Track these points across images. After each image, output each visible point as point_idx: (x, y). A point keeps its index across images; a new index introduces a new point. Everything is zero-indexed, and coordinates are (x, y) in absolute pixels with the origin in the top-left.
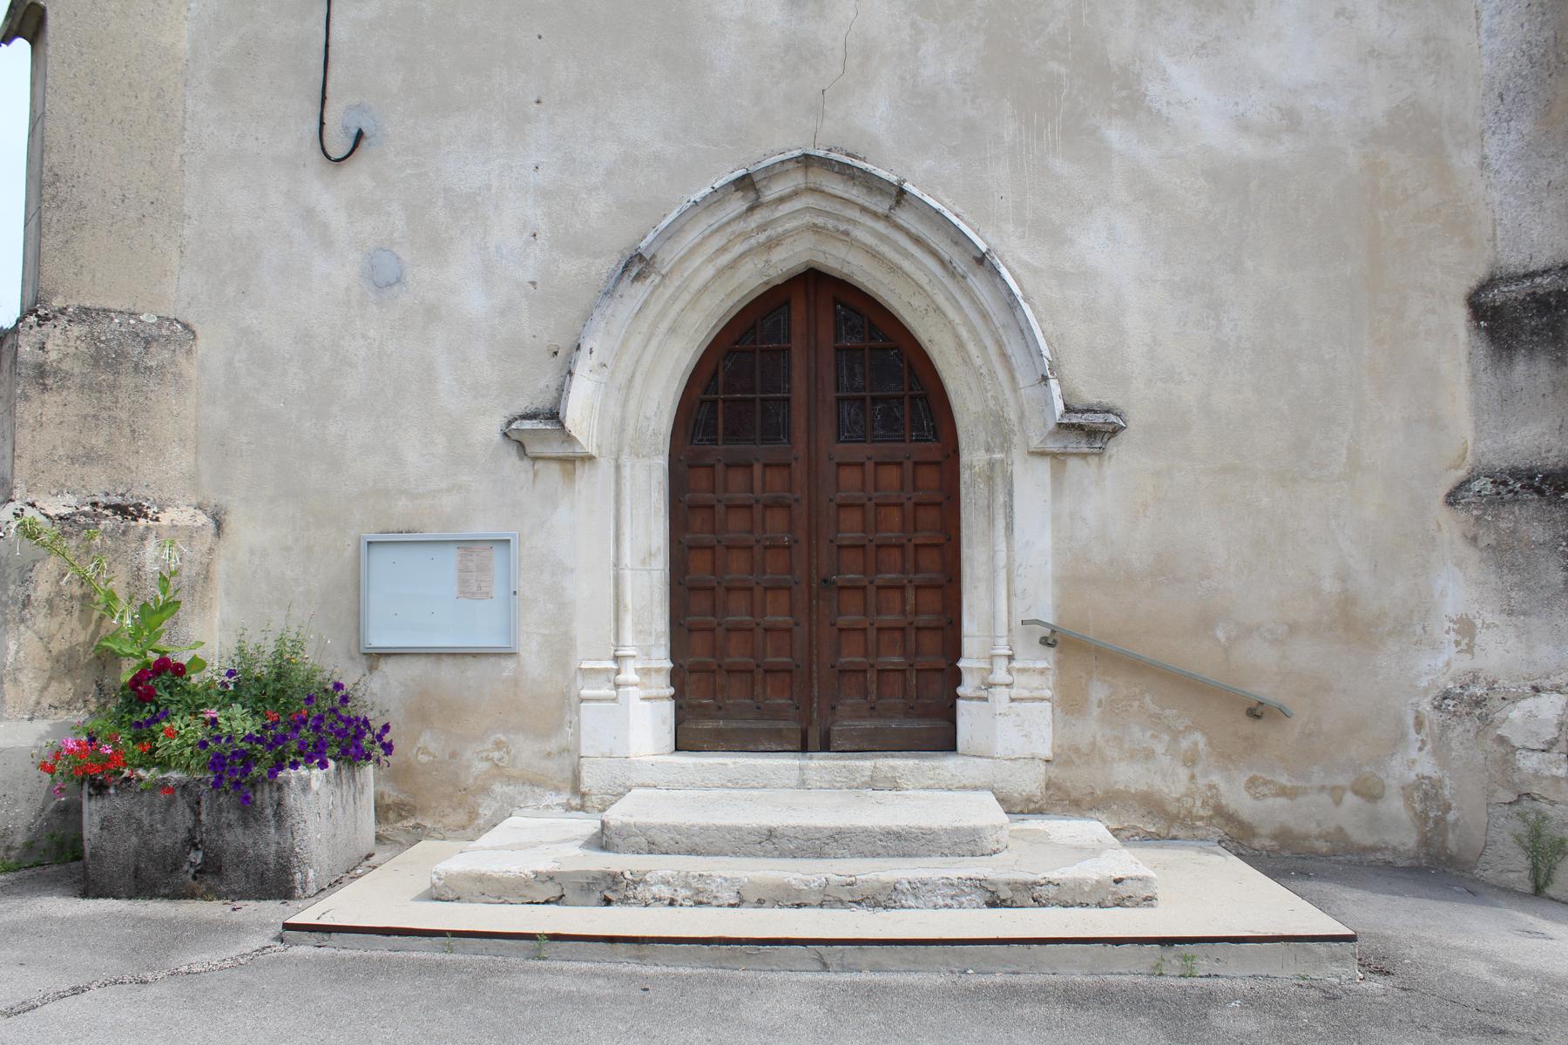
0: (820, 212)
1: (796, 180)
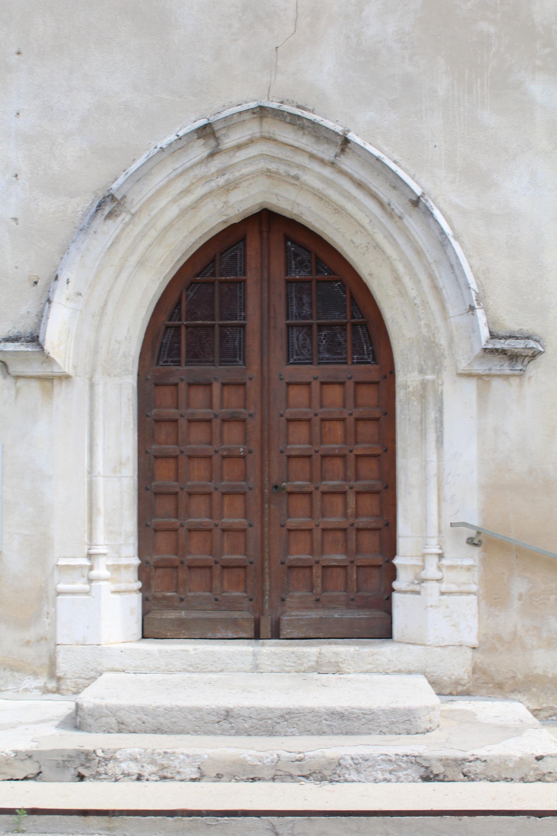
0: (273, 158)
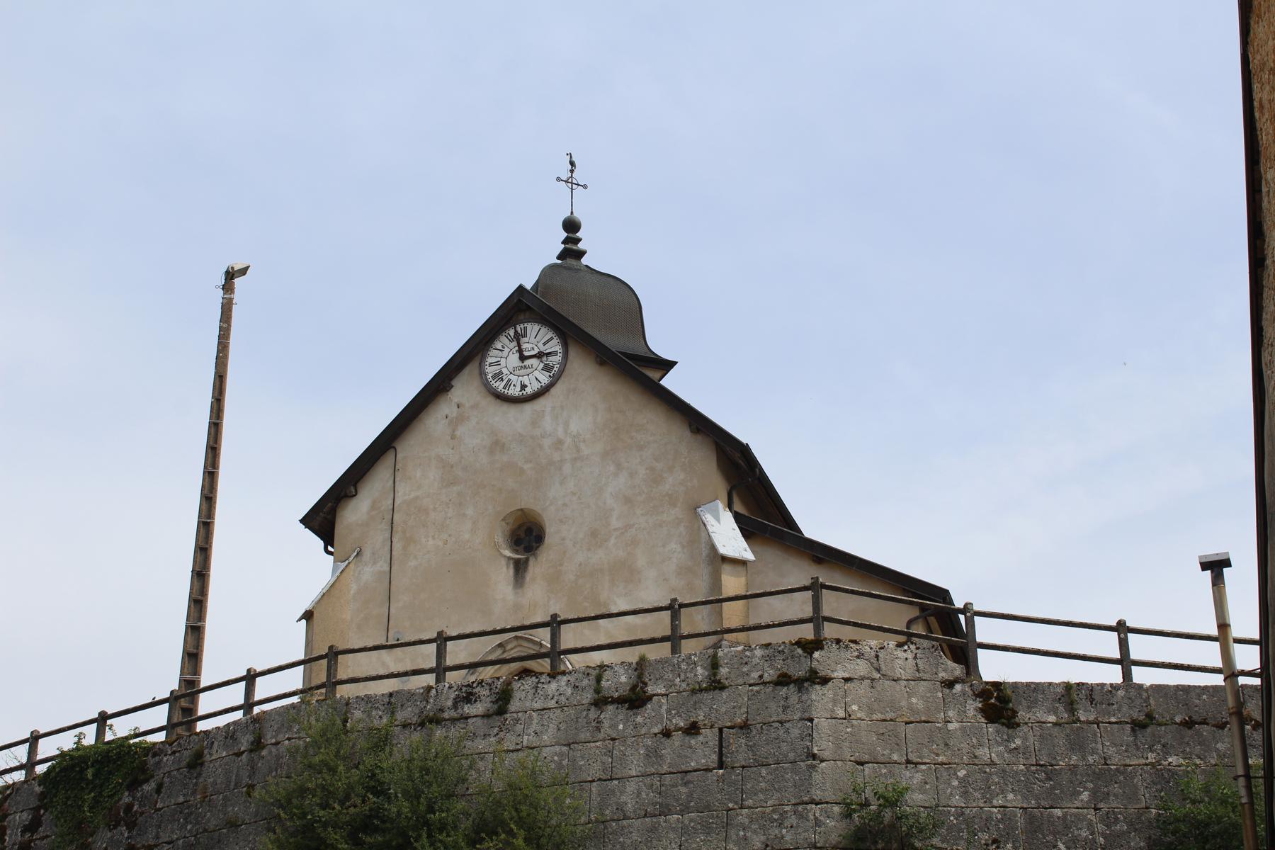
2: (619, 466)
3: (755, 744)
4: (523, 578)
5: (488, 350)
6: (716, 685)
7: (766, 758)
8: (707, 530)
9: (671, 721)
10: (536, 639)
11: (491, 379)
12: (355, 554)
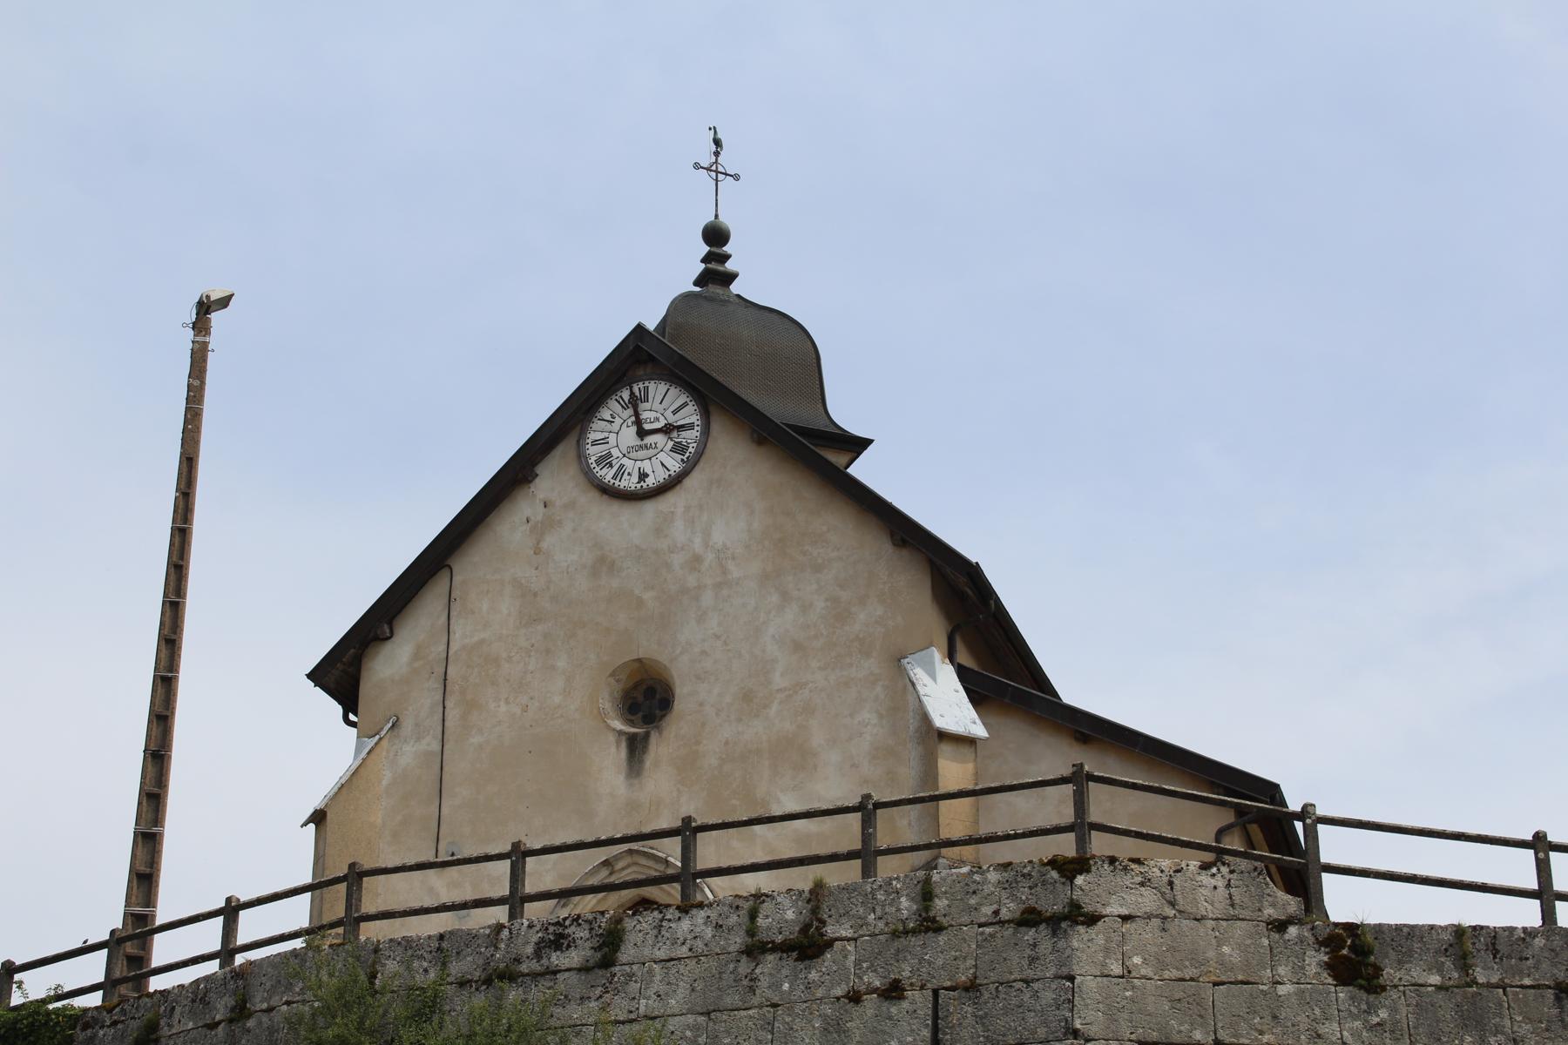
1: (628, 860)
2: (785, 596)
3: (986, 1014)
4: (641, 762)
5: (590, 421)
6: (929, 925)
7: (1004, 1035)
8: (917, 692)
9: (861, 978)
10: (660, 854)
11: (594, 465)
12: (390, 724)
